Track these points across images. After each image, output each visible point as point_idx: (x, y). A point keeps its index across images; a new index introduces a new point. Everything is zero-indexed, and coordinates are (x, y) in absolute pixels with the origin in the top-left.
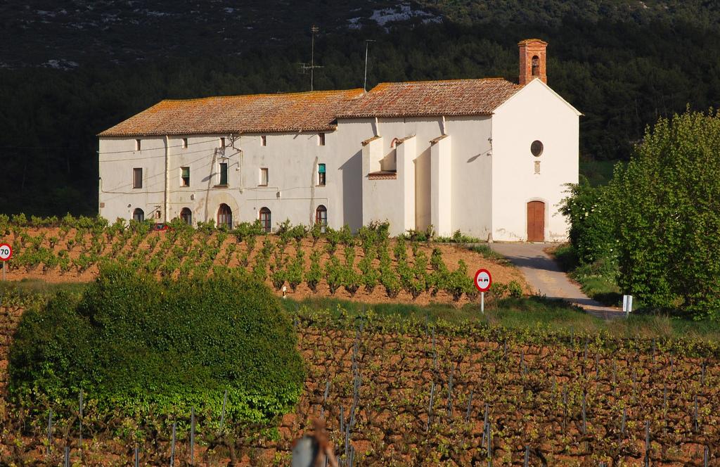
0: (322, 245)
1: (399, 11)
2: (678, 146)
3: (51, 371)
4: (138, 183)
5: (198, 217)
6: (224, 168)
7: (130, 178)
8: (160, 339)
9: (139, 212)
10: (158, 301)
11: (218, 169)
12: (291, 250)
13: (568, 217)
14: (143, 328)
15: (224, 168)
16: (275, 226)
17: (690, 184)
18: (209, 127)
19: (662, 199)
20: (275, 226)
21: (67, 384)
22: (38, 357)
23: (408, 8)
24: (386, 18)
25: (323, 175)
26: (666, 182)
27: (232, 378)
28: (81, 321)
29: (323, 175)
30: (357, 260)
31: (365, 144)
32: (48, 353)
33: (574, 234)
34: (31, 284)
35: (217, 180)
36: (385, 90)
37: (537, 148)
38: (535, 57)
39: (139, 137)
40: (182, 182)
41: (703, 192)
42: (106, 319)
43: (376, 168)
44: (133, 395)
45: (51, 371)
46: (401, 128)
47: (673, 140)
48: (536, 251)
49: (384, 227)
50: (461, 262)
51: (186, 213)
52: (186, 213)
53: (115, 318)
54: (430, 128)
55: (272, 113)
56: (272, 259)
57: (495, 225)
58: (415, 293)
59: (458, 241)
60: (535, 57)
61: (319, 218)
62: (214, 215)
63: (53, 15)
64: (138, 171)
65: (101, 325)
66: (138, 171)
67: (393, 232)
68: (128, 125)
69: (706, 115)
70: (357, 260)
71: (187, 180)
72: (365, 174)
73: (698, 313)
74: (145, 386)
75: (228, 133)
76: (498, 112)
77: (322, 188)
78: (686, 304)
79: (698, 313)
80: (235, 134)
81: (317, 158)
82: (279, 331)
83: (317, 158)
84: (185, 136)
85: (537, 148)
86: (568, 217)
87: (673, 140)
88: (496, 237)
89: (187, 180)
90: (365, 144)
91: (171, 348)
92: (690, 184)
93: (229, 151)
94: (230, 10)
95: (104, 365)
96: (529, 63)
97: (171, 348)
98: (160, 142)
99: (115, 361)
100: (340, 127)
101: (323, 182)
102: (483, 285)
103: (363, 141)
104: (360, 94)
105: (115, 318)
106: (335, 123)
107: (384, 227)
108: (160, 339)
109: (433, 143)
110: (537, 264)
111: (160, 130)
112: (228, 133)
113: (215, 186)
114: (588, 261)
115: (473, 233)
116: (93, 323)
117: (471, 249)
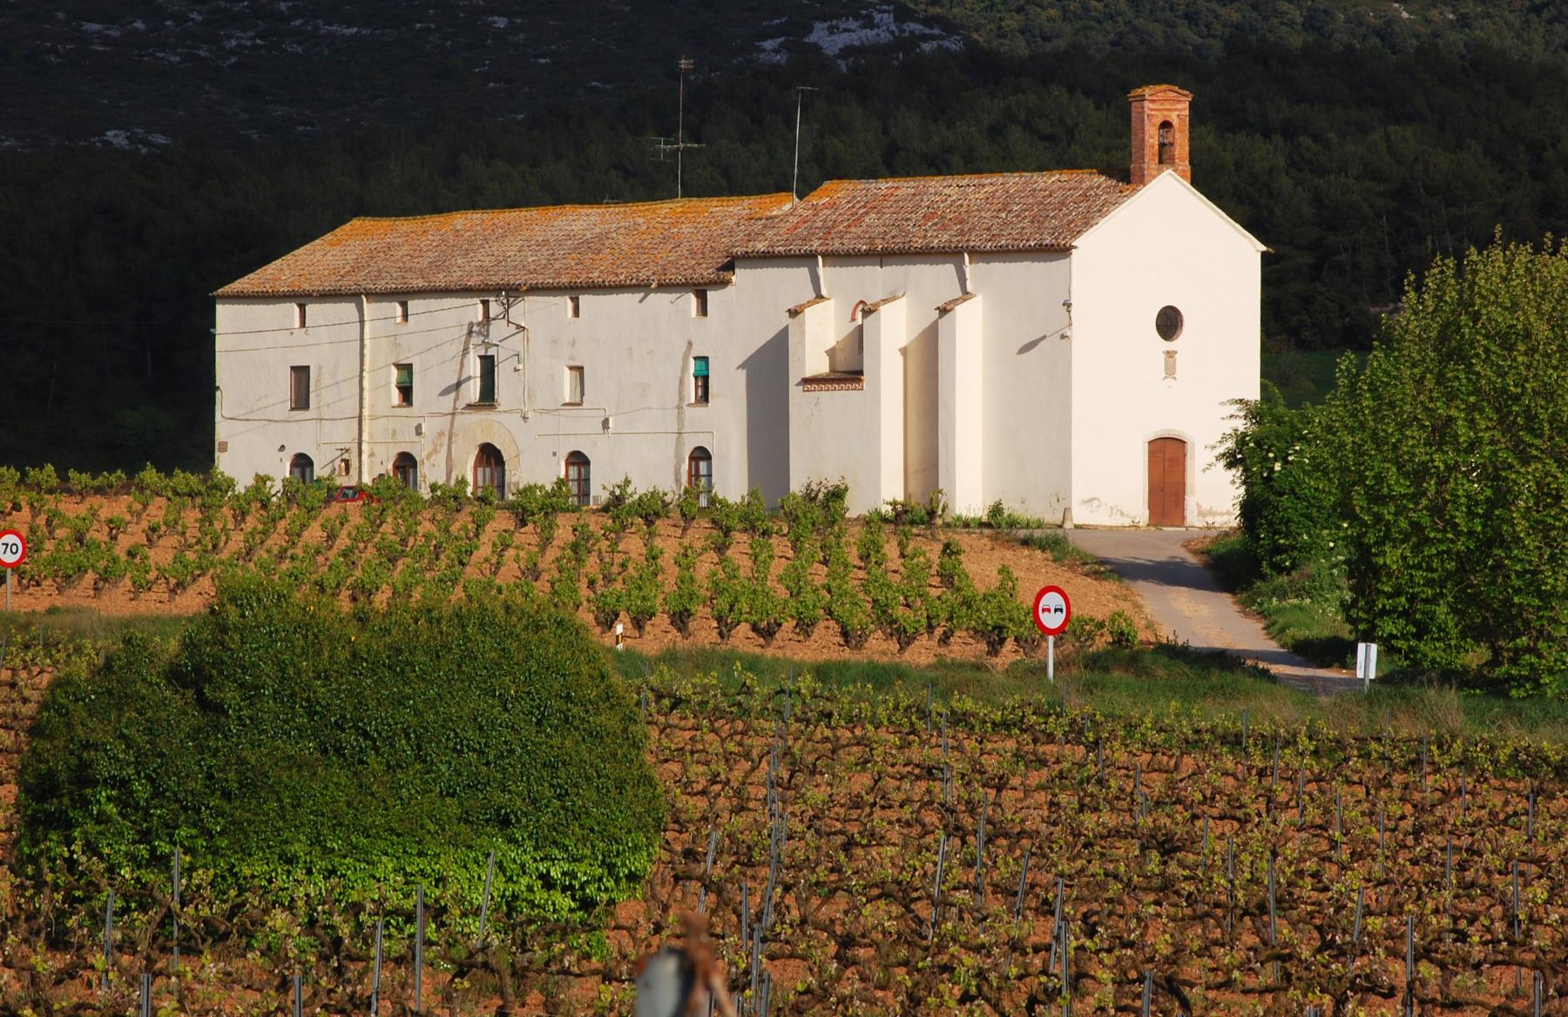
0: (700, 533)
1: (869, 23)
2: (1476, 317)
3: (111, 809)
4: (301, 400)
5: (431, 473)
6: (488, 364)
7: (284, 387)
8: (350, 738)
9: (302, 462)
10: (343, 655)
11: (474, 367)
12: (633, 545)
13: (1237, 472)
14: (311, 714)
15: (488, 364)
16: (599, 492)
17: (1502, 401)
18: (455, 277)
19: (1441, 434)
20: (599, 492)
21: (145, 836)
22: (83, 778)
23: (888, 18)
24: (841, 40)
25: (703, 381)
26: (1451, 397)
27: (505, 823)
28: (177, 699)
29: (703, 381)
30: (778, 567)
31: (794, 313)
32: (104, 768)
33: (1251, 509)
34: (69, 619)
35: (473, 391)
36: (839, 195)
37: (1169, 322)
38: (1166, 125)
39: (302, 298)
40: (396, 396)
41: (1531, 417)
42: (230, 695)
43: (818, 365)
44: (291, 860)
45: (111, 809)
46: (872, 279)
47: (1464, 304)
48: (1168, 547)
49: (837, 494)
50: (1004, 571)
51: (406, 463)
52: (406, 463)
53: (251, 692)
54: (936, 279)
55: (593, 245)
56: (591, 564)
57: (1078, 494)
58: (905, 638)
59: (997, 525)
60: (1166, 125)
61: (694, 475)
62: (467, 467)
63: (114, 33)
64: (301, 374)
65: (219, 709)
66: (301, 374)
67: (856, 506)
68: (280, 272)
69: (1538, 250)
70: (778, 567)
71: (406, 392)
72: (794, 378)
73: (1520, 681)
74: (317, 841)
75: (496, 290)
76: (1085, 245)
77: (701, 411)
78: (1495, 662)
79: (1520, 681)
80: (513, 292)
81: (690, 344)
82: (607, 720)
83: (690, 344)
84: (402, 296)
85: (1169, 322)
86: (1237, 472)
87: (1464, 304)
88: (1080, 516)
89: (406, 392)
90: (794, 313)
91: (372, 758)
92: (1502, 401)
93: (498, 330)
94: (501, 22)
95: (227, 795)
96: (1152, 138)
97: (372, 758)
98: (347, 309)
99: (252, 785)
100: (741, 276)
101: (704, 397)
102: (1052, 621)
103: (792, 306)
104: (785, 206)
105: (251, 692)
106: (730, 267)
107: (837, 494)
108: (350, 738)
109: (944, 311)
110: (1169, 574)
111: (348, 284)
112: (496, 290)
113: (469, 406)
114: (1280, 569)
115: (1029, 507)
116: (203, 704)
117: (1026, 543)
